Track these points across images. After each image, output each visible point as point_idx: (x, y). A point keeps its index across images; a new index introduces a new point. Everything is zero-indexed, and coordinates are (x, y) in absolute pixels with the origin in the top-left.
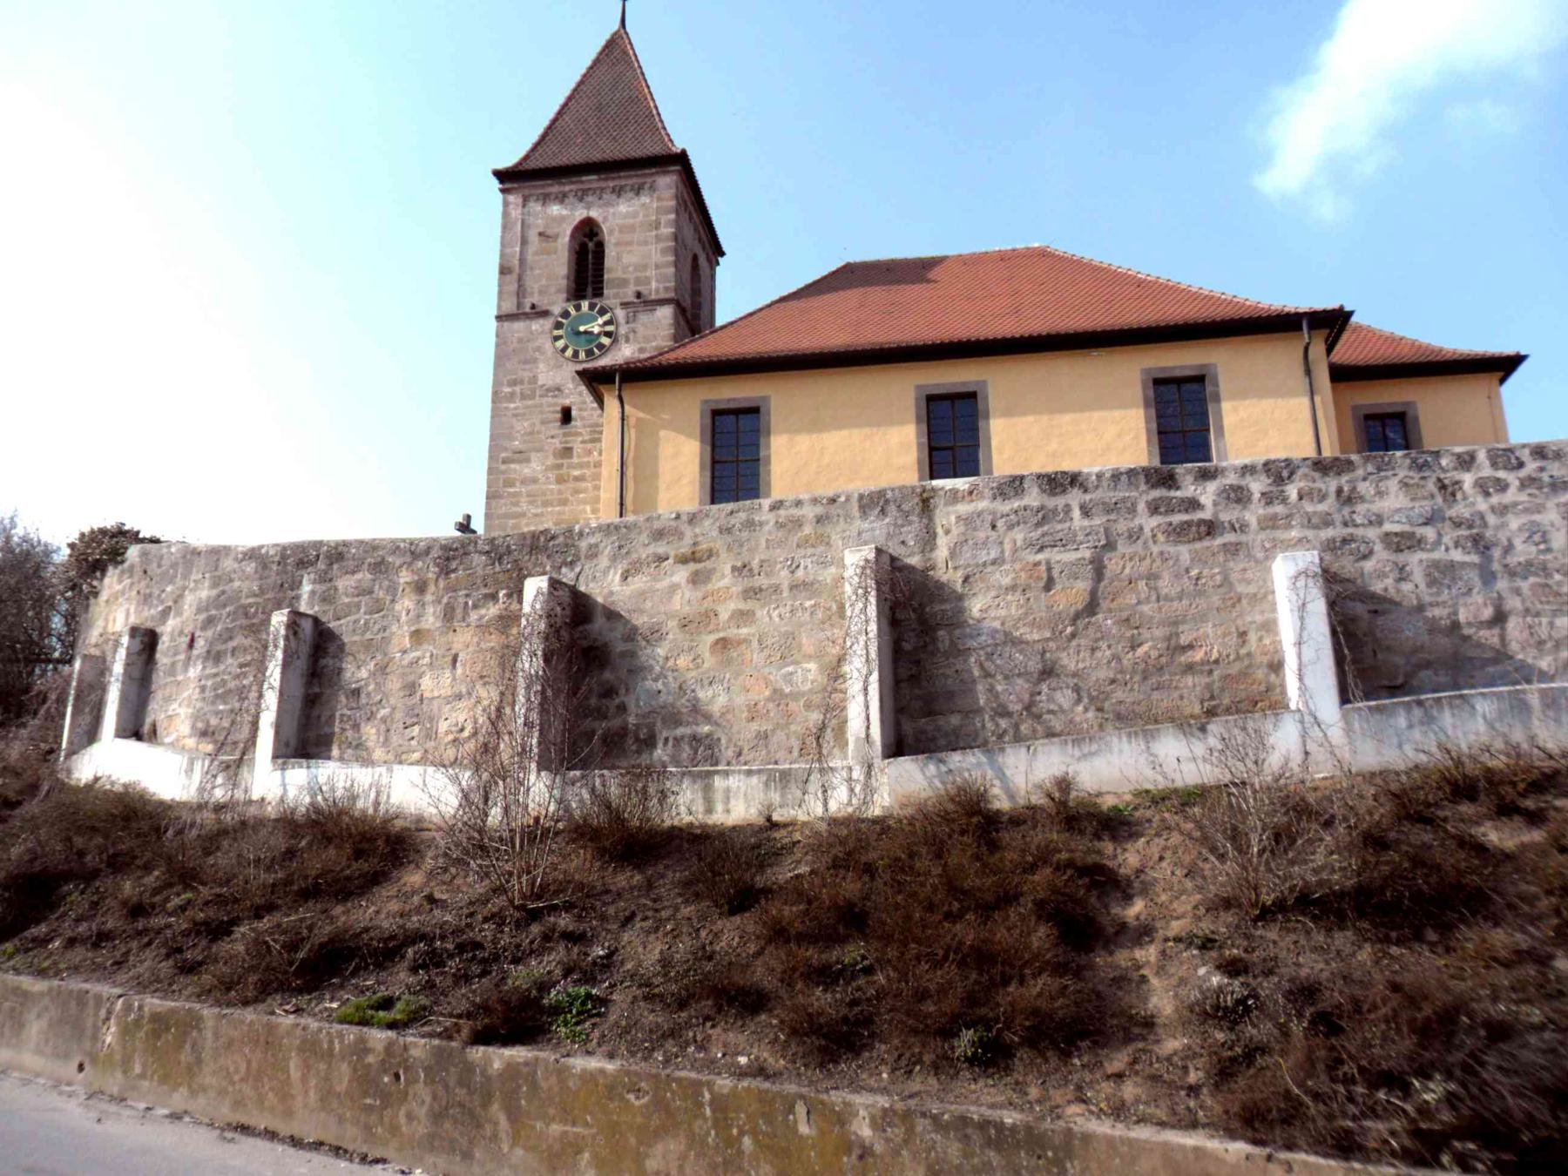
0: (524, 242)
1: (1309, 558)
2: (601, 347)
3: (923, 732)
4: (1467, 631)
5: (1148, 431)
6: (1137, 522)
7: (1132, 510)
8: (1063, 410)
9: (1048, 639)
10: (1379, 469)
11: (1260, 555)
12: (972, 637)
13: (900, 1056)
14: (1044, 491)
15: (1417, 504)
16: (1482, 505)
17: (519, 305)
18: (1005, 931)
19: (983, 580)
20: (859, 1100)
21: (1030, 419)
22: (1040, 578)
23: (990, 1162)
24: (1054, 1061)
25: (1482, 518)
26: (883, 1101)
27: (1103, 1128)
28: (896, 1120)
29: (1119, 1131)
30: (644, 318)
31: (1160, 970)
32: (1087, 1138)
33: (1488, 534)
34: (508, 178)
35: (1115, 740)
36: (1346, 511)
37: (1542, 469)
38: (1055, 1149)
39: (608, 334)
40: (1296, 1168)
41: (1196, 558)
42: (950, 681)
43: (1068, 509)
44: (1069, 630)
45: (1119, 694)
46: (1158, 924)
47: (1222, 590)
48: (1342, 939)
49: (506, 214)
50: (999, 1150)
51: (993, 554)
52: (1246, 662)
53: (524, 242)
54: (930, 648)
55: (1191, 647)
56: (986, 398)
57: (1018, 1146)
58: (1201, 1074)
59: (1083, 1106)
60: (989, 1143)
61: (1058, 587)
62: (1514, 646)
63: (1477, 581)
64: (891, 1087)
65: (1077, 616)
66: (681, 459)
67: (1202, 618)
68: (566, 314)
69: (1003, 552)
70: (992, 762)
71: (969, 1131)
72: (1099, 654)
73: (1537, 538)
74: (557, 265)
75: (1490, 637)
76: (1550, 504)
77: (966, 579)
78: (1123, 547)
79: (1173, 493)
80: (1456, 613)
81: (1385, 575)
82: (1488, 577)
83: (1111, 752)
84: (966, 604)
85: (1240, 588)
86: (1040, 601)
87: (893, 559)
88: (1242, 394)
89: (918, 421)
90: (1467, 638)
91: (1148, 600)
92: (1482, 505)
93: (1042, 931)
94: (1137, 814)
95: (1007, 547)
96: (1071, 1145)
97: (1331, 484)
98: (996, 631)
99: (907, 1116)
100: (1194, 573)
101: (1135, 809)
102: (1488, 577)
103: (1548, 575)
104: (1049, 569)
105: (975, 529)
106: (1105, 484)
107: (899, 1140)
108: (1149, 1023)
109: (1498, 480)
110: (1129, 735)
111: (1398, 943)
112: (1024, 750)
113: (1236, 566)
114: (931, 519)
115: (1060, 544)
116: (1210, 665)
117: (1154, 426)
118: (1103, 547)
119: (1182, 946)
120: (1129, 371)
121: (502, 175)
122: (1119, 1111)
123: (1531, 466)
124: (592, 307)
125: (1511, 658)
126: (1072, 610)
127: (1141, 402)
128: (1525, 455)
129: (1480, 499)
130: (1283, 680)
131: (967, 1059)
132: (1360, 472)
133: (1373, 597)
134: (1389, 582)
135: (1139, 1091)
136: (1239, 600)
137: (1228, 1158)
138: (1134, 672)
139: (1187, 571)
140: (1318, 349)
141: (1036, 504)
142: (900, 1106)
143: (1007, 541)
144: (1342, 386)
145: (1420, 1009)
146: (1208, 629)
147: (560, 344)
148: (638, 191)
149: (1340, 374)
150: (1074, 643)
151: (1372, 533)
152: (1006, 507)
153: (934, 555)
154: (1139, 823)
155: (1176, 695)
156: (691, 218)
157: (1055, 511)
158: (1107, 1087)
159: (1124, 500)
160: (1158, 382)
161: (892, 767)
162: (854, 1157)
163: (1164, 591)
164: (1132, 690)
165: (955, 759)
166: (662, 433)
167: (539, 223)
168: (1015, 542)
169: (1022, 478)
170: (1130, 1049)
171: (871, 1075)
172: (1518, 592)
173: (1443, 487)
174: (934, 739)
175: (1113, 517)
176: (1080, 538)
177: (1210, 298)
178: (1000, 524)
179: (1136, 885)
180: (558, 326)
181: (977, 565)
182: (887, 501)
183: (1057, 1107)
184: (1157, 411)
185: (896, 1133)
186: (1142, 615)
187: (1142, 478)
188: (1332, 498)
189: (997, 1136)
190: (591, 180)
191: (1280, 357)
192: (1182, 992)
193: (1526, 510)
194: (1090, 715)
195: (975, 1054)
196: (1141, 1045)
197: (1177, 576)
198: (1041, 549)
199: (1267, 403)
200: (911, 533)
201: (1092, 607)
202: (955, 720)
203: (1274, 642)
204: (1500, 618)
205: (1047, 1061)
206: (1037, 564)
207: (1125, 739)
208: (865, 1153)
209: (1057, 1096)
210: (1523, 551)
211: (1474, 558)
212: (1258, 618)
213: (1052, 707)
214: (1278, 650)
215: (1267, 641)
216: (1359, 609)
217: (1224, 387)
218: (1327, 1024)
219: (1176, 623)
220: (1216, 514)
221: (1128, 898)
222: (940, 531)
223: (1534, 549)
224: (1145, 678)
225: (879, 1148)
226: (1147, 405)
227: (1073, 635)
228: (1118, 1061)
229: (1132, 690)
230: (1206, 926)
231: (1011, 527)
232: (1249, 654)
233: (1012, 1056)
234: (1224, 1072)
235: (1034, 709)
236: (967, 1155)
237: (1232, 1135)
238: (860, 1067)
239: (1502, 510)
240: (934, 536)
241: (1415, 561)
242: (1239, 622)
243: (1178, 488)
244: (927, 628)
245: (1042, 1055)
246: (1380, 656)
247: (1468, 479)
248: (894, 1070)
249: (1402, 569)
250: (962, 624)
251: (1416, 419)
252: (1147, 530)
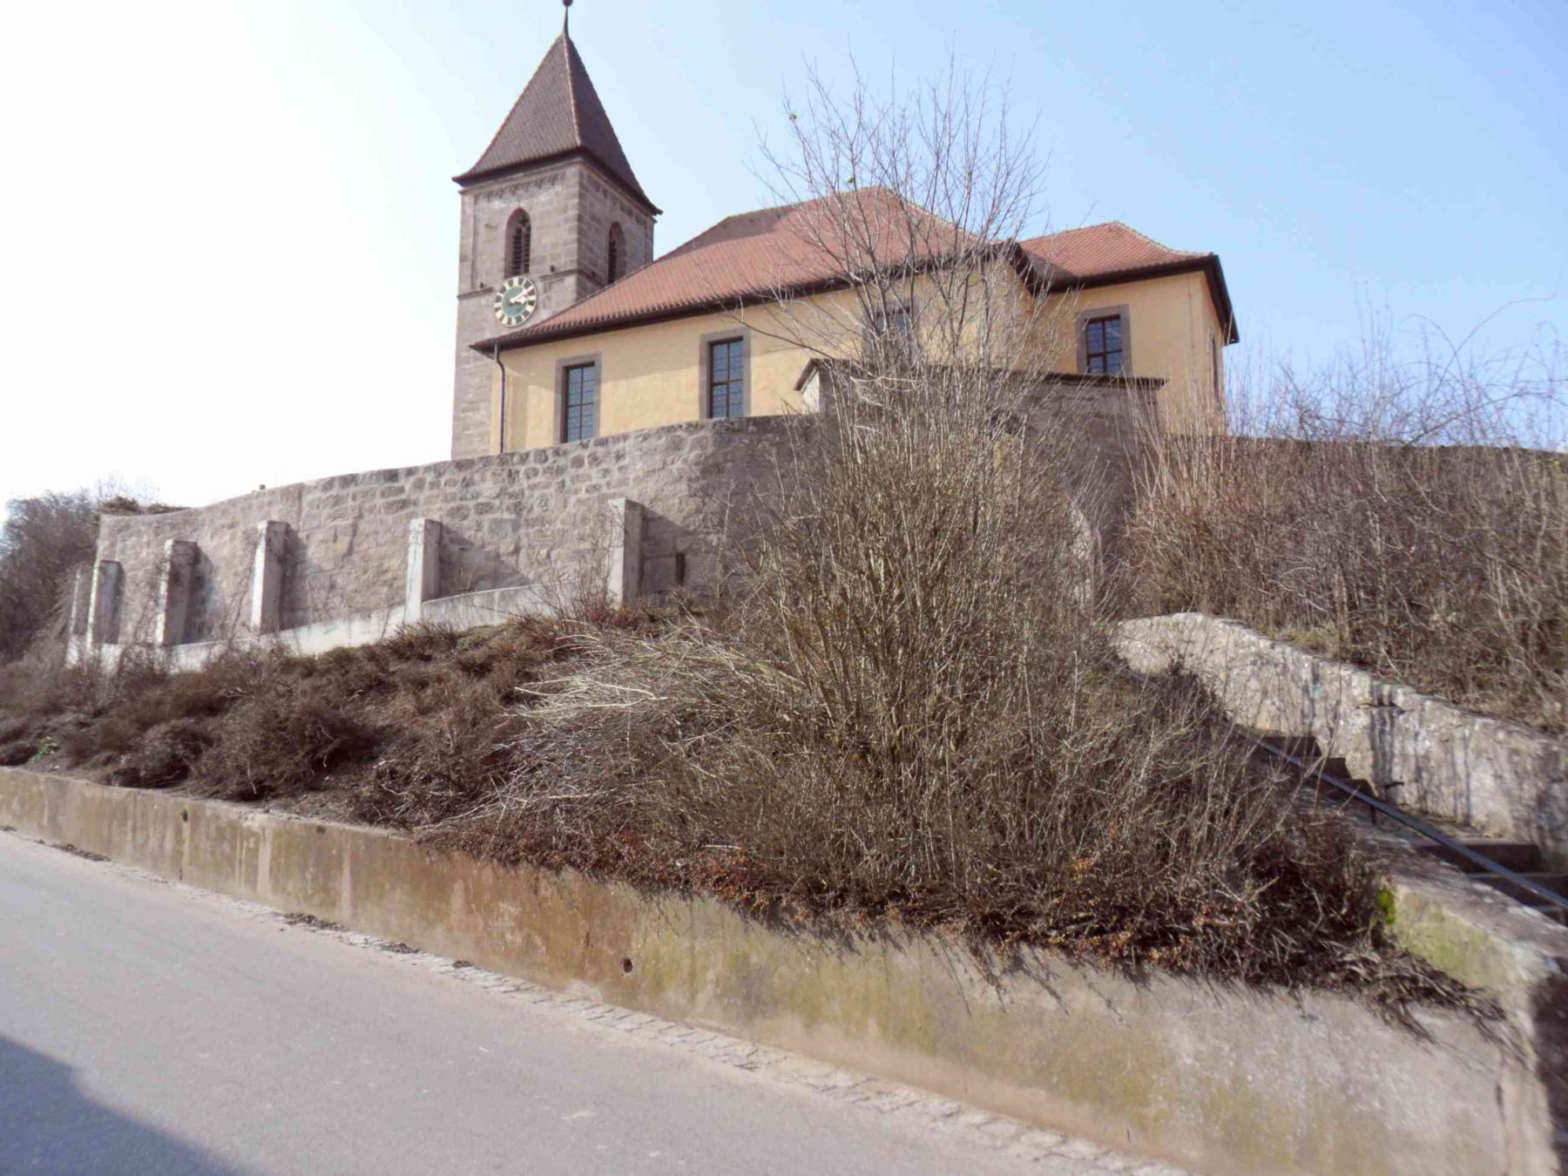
0: (476, 233)
2: (526, 313)
16: (525, 484)
17: (473, 285)
30: (556, 286)
34: (467, 180)
39: (531, 303)
49: (463, 211)
53: (476, 233)
65: (344, 556)
66: (542, 404)
68: (503, 290)
74: (497, 250)
75: (511, 561)
89: (701, 363)
102: (516, 526)
115: (341, 516)
121: (461, 180)
124: (520, 282)
147: (499, 314)
148: (553, 181)
156: (605, 193)
166: (531, 387)
167: (484, 218)
172: (527, 535)
180: (498, 299)
190: (519, 177)
201: (350, 551)
204: (517, 551)
211: (513, 516)
251: (1128, 321)
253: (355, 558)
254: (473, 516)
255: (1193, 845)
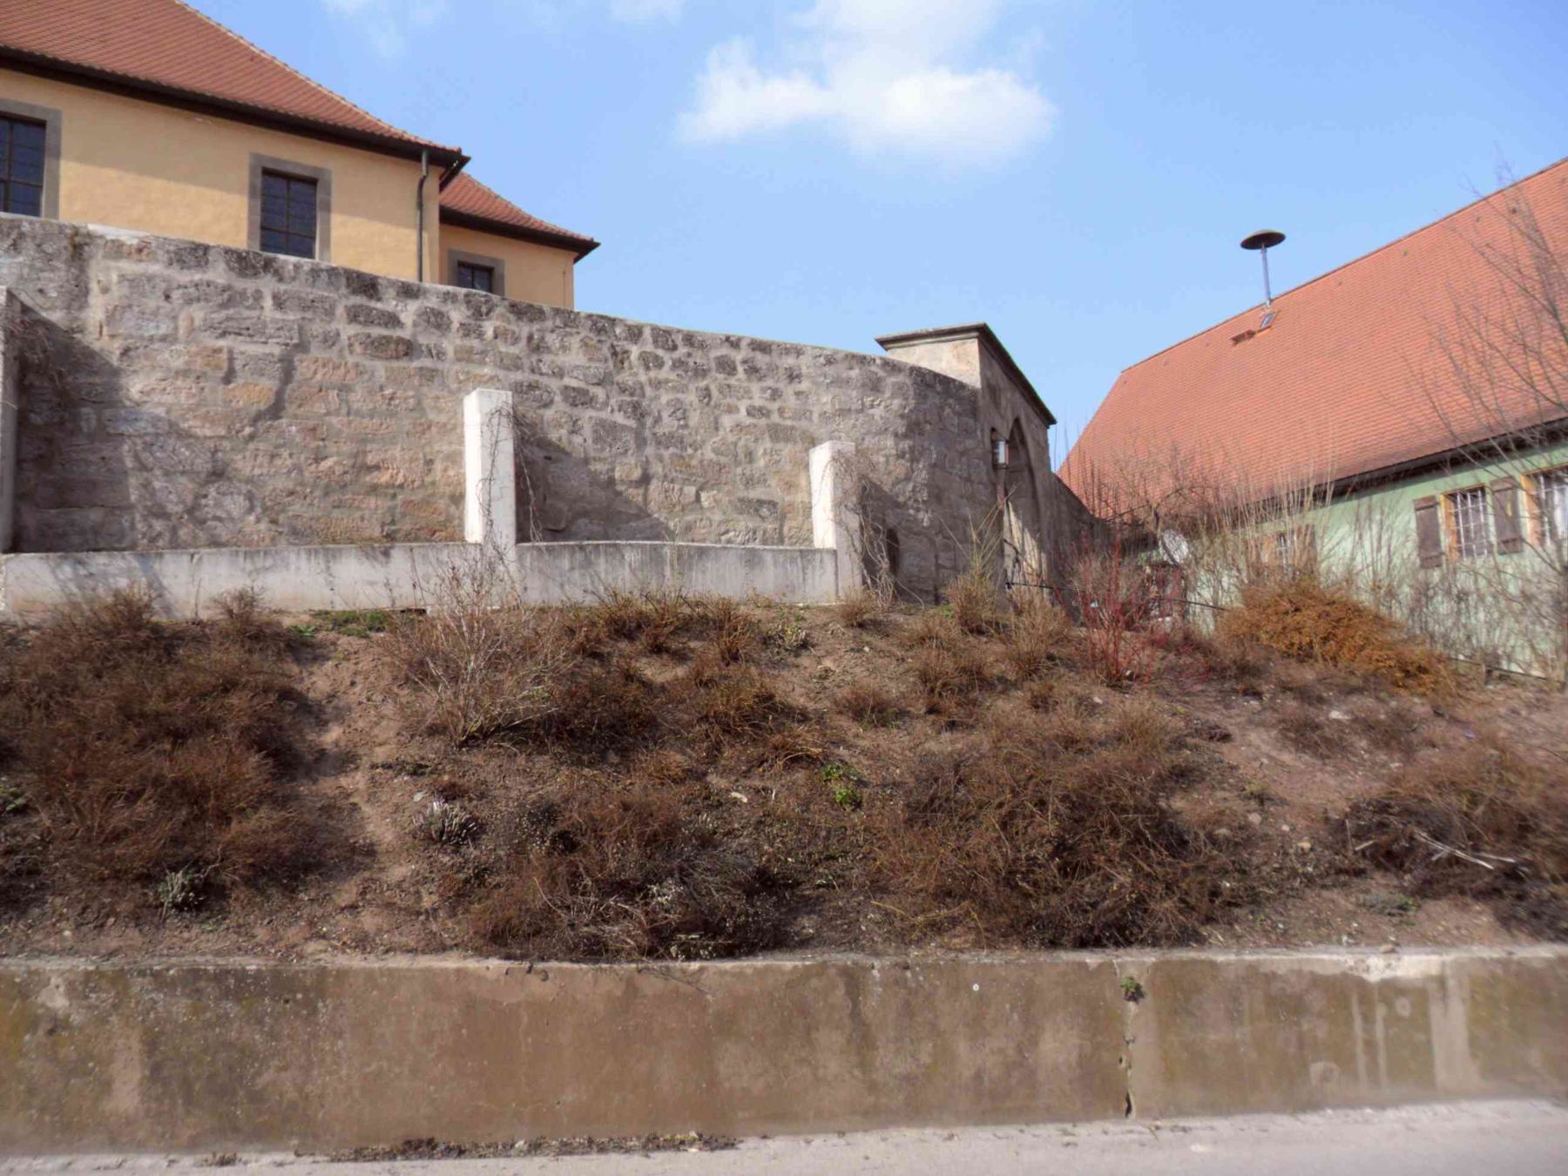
1: (504, 398)
3: (50, 526)
4: (620, 488)
5: (251, 223)
6: (334, 326)
7: (330, 313)
8: (155, 173)
9: (223, 438)
10: (566, 325)
11: (454, 386)
12: (126, 420)
13: (84, 909)
14: (232, 269)
15: (593, 365)
18: (201, 762)
19: (147, 357)
20: (51, 965)
21: (112, 173)
22: (218, 367)
23: (227, 1015)
24: (277, 897)
25: (642, 388)
26: (83, 964)
27: (354, 961)
28: (104, 984)
29: (373, 963)
31: (372, 798)
32: (342, 974)
33: (645, 403)
35: (293, 557)
36: (534, 358)
37: (689, 355)
38: (306, 990)
40: (551, 975)
41: (392, 378)
42: (93, 469)
43: (258, 296)
44: (248, 430)
45: (297, 507)
46: (361, 751)
47: (415, 414)
48: (542, 763)
50: (238, 1000)
51: (164, 329)
52: (430, 491)
54: (69, 426)
55: (377, 467)
56: (58, 131)
57: (263, 994)
58: (435, 898)
59: (324, 942)
60: (226, 994)
61: (240, 381)
62: (653, 506)
63: (632, 445)
64: (81, 947)
67: (393, 441)
69: (176, 328)
70: (147, 570)
71: (202, 984)
72: (278, 462)
73: (679, 414)
75: (635, 494)
76: (692, 387)
77: (125, 352)
78: (316, 351)
79: (373, 304)
80: (613, 470)
81: (561, 426)
82: (641, 442)
83: (287, 566)
84: (123, 381)
85: (432, 416)
86: (217, 394)
87: (25, 309)
88: (353, 210)
90: (619, 494)
91: (337, 412)
92: (643, 378)
93: (254, 759)
94: (320, 636)
95: (183, 324)
96: (323, 983)
97: (524, 329)
98: (160, 419)
99: (119, 978)
100: (388, 392)
101: (317, 630)
102: (641, 442)
103: (684, 449)
104: (231, 359)
105: (143, 295)
106: (303, 277)
107: (107, 1005)
108: (370, 851)
109: (657, 357)
110: (309, 552)
111: (591, 765)
112: (186, 558)
113: (430, 392)
114: (82, 270)
116: (394, 489)
117: (258, 219)
118: (296, 346)
119: (390, 772)
120: (246, 149)
122: (362, 943)
123: (682, 350)
125: (649, 516)
126: (254, 409)
127: (246, 189)
128: (679, 339)
129: (641, 371)
130: (462, 513)
131: (176, 906)
132: (549, 324)
133: (550, 443)
134: (564, 432)
135: (378, 920)
136: (429, 427)
137: (489, 975)
138: (315, 486)
139: (381, 388)
140: (432, 184)
141: (221, 281)
142: (106, 966)
143: (182, 316)
144: (446, 226)
145: (647, 825)
146: (397, 452)
149: (450, 218)
150: (251, 446)
151: (554, 384)
152: (185, 277)
153: (83, 315)
154: (322, 645)
155: (358, 514)
157: (243, 294)
158: (344, 921)
159: (323, 299)
160: (267, 173)
161: (12, 565)
162: (41, 1032)
163: (355, 406)
164: (311, 504)
165: (99, 561)
168: (192, 320)
169: (206, 248)
170: (357, 879)
171: (48, 935)
172: (661, 459)
173: (615, 354)
174: (64, 535)
175: (309, 315)
176: (270, 331)
177: (327, 99)
178: (176, 295)
179: (329, 710)
181: (142, 338)
182: (22, 235)
183: (294, 946)
184: (264, 204)
185: (106, 997)
186: (330, 426)
187: (343, 281)
188: (524, 342)
189: (236, 986)
191: (397, 181)
192: (403, 818)
193: (674, 388)
194: (263, 526)
195: (185, 900)
196: (367, 874)
197: (371, 392)
198: (224, 334)
199: (378, 226)
200: (55, 280)
201: (276, 410)
202: (95, 515)
203: (458, 474)
204: (645, 480)
205: (268, 898)
206: (218, 351)
207: (303, 556)
208: (57, 1026)
209: (293, 934)
210: (668, 424)
211: (632, 423)
212: (445, 448)
213: (219, 513)
214: (461, 482)
215: (451, 473)
216: (539, 454)
217: (335, 198)
218: (567, 842)
219: (364, 441)
220: (414, 335)
221: (322, 724)
222: (94, 287)
223: (676, 423)
224: (327, 494)
225: (76, 1019)
226: (252, 195)
227: (252, 437)
228: (347, 892)
229: (311, 504)
230: (412, 753)
231: (189, 301)
232: (433, 483)
233: (225, 897)
234: (460, 895)
235: (198, 514)
236: (196, 1011)
237: (480, 952)
238: (31, 927)
239: (657, 384)
240: (86, 292)
241: (587, 416)
242: (427, 449)
243: (379, 300)
244: (67, 402)
245: (261, 891)
246: (548, 502)
247: (635, 351)
248: (78, 926)
249: (575, 422)
250: (115, 404)
251: (502, 277)
252: (344, 337)
253: (289, 426)
254: (560, 404)
255: (458, 813)
